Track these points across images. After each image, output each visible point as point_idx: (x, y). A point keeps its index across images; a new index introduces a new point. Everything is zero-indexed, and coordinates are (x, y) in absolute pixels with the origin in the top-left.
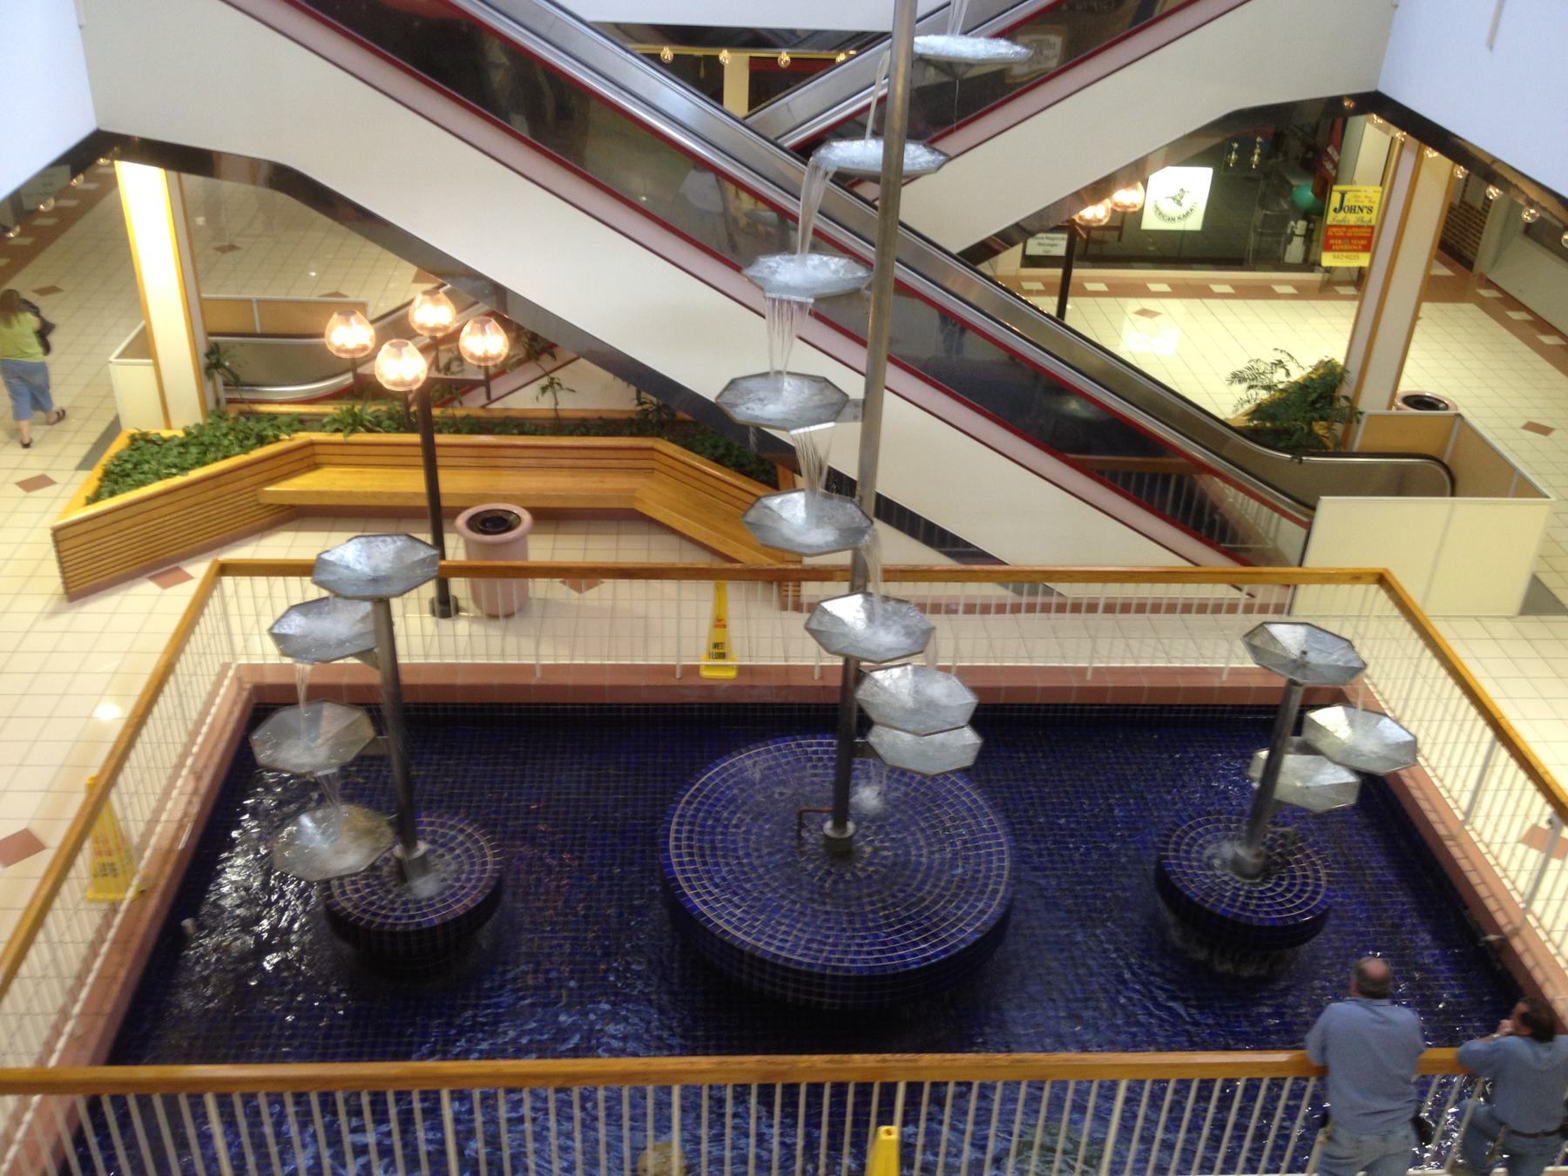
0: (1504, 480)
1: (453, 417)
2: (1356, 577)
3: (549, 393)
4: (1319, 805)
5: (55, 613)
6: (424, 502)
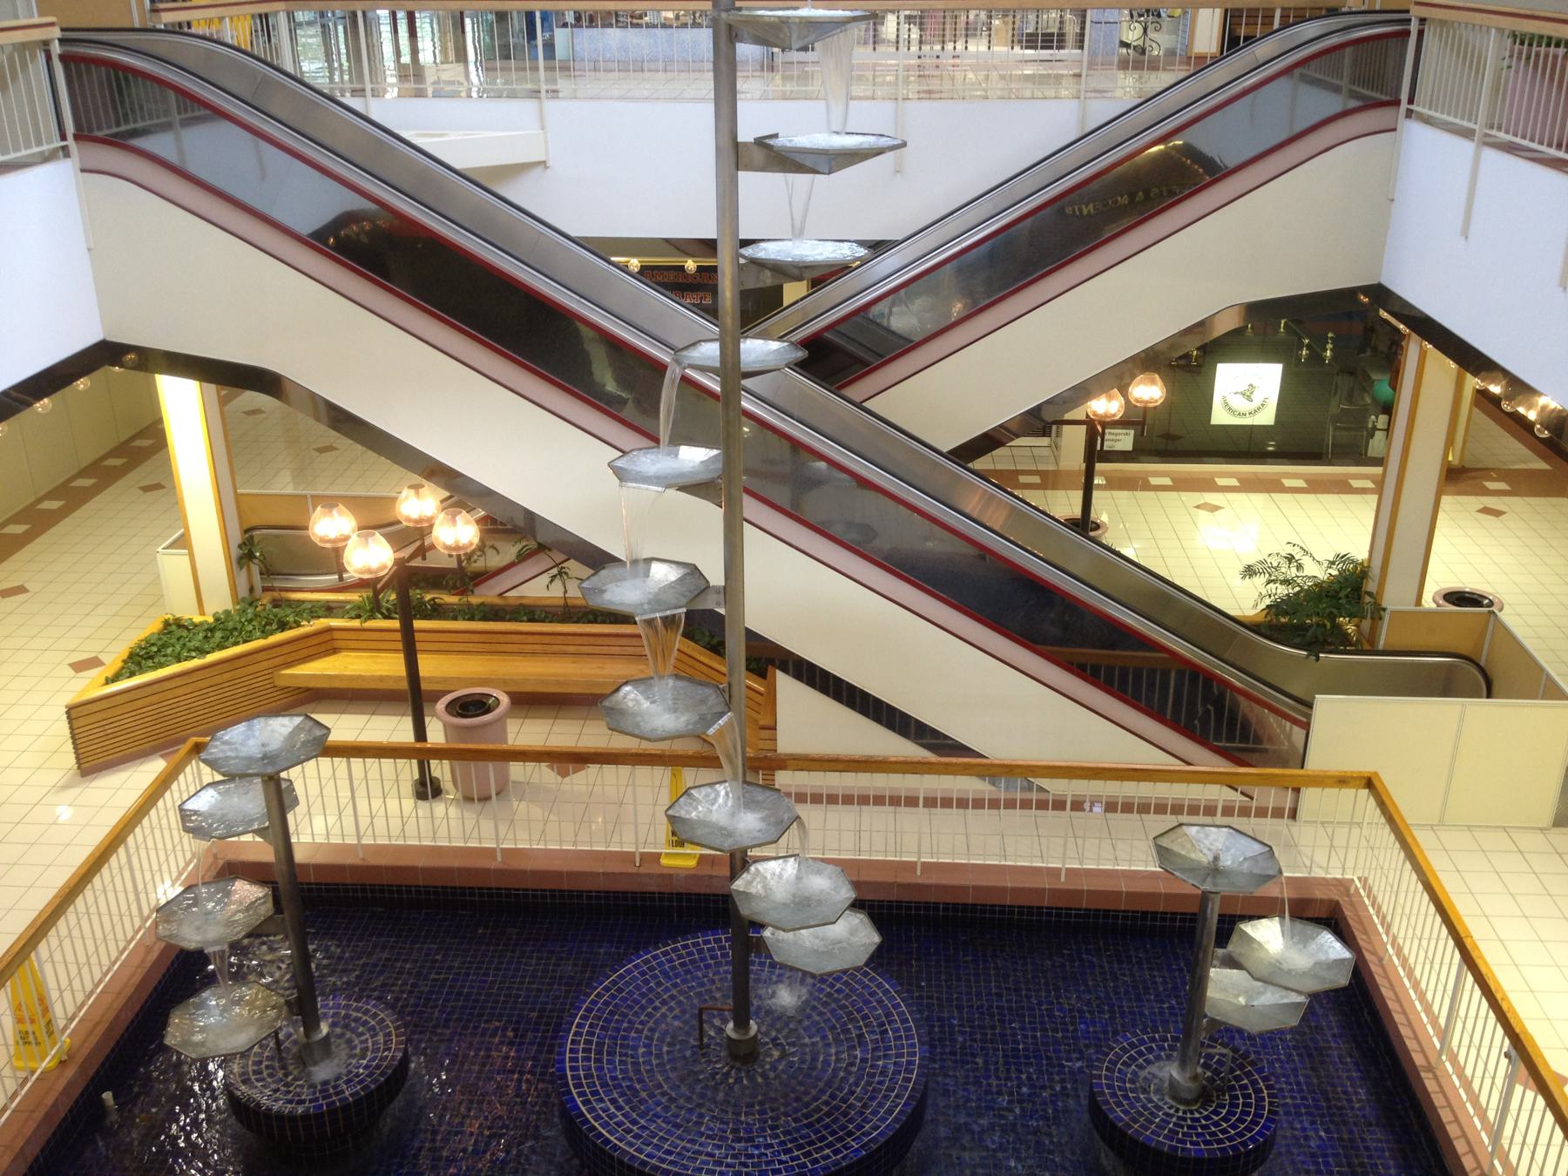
0: (1533, 682)
1: (469, 605)
2: (1342, 781)
3: (558, 582)
4: (1254, 1025)
5: (66, 787)
6: (404, 685)
